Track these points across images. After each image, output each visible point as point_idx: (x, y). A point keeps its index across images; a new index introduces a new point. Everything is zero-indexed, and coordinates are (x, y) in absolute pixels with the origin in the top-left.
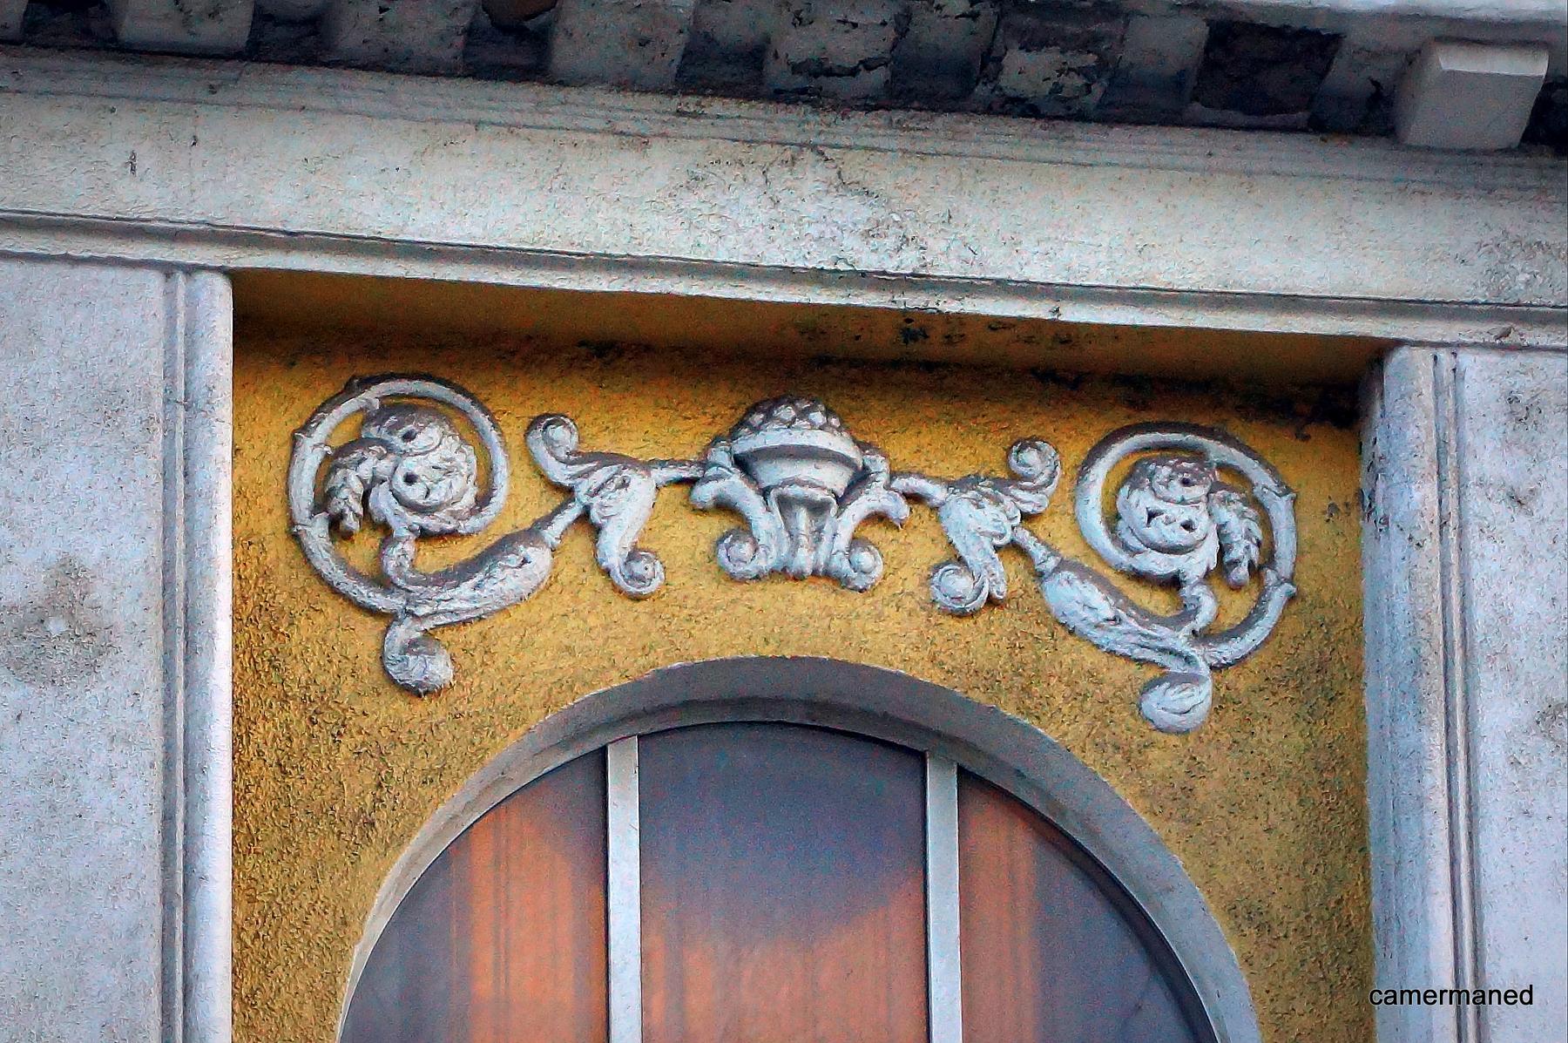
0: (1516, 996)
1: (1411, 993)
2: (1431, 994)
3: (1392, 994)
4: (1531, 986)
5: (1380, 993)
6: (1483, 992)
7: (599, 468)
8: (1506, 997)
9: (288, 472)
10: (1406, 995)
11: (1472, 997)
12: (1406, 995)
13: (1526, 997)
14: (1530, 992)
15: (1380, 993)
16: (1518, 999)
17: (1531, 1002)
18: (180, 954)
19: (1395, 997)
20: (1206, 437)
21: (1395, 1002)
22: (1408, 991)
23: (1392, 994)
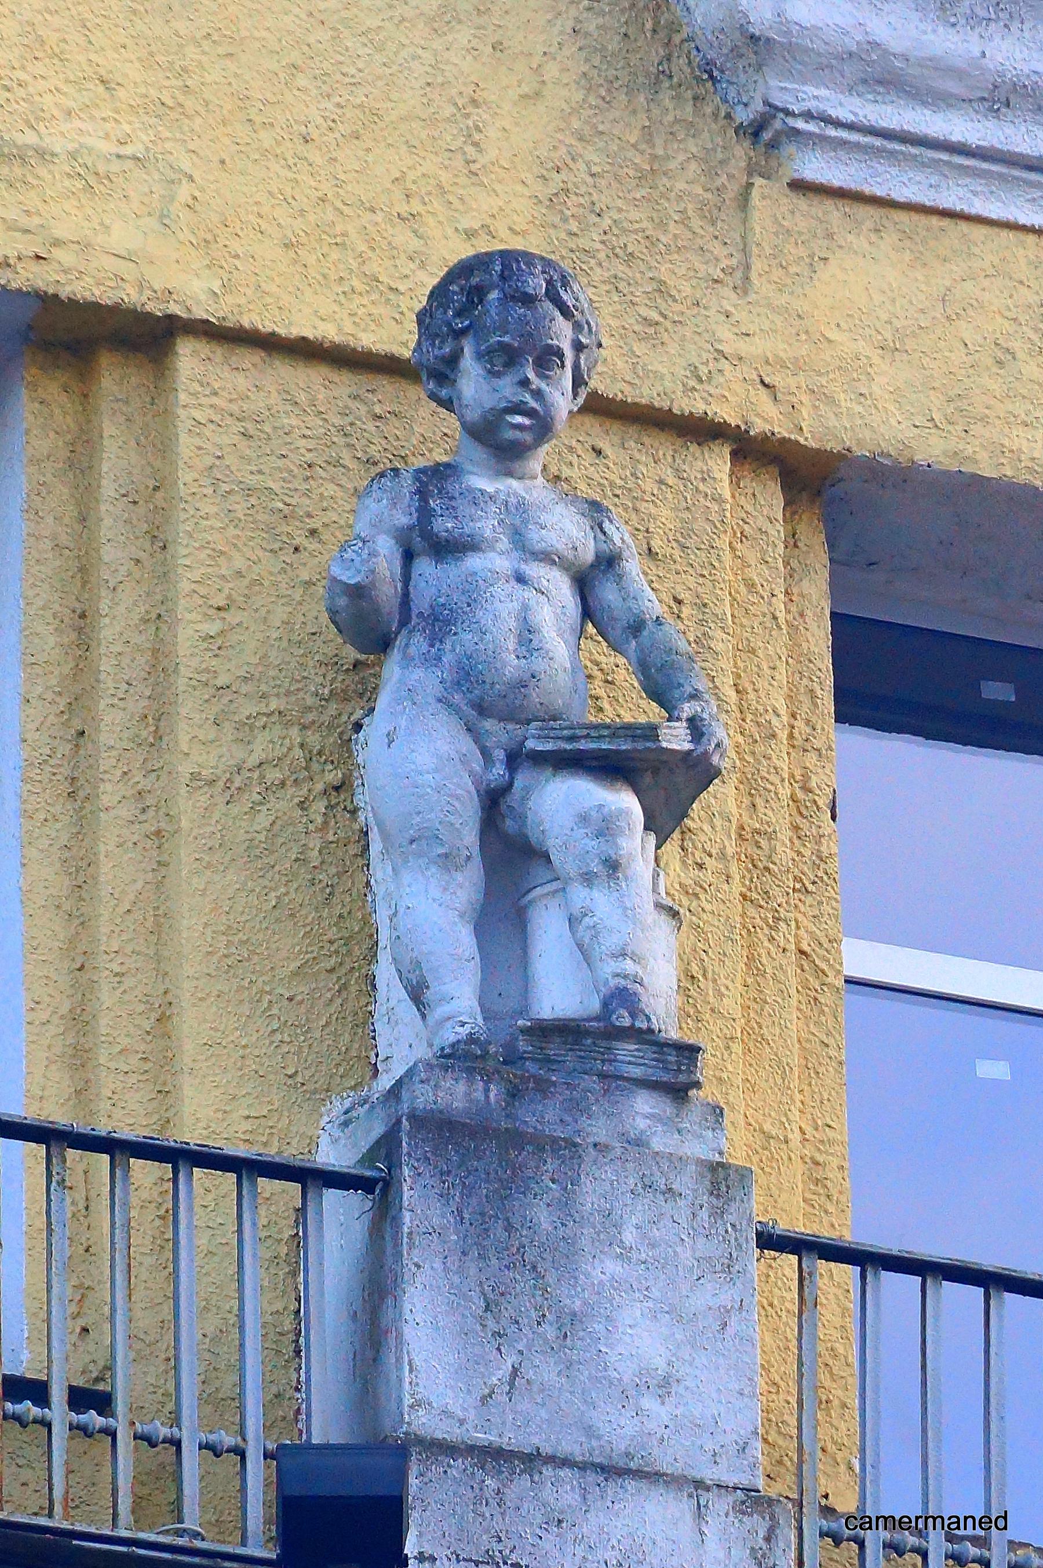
0: (991, 1522)
1: (935, 1519)
2: (906, 1520)
3: (955, 1520)
4: (1006, 1512)
5: (856, 1519)
6: (958, 1518)
7: (571, 287)
8: (980, 1523)
9: (299, 1242)
10: (881, 1521)
11: (947, 1522)
12: (881, 1521)
13: (1001, 1523)
14: (1005, 1518)
15: (856, 1519)
16: (993, 1525)
17: (1005, 1528)
18: (98, 1545)
19: (958, 1522)
20: (565, 750)
21: (870, 1528)
22: (883, 1517)
23: (867, 1520)
